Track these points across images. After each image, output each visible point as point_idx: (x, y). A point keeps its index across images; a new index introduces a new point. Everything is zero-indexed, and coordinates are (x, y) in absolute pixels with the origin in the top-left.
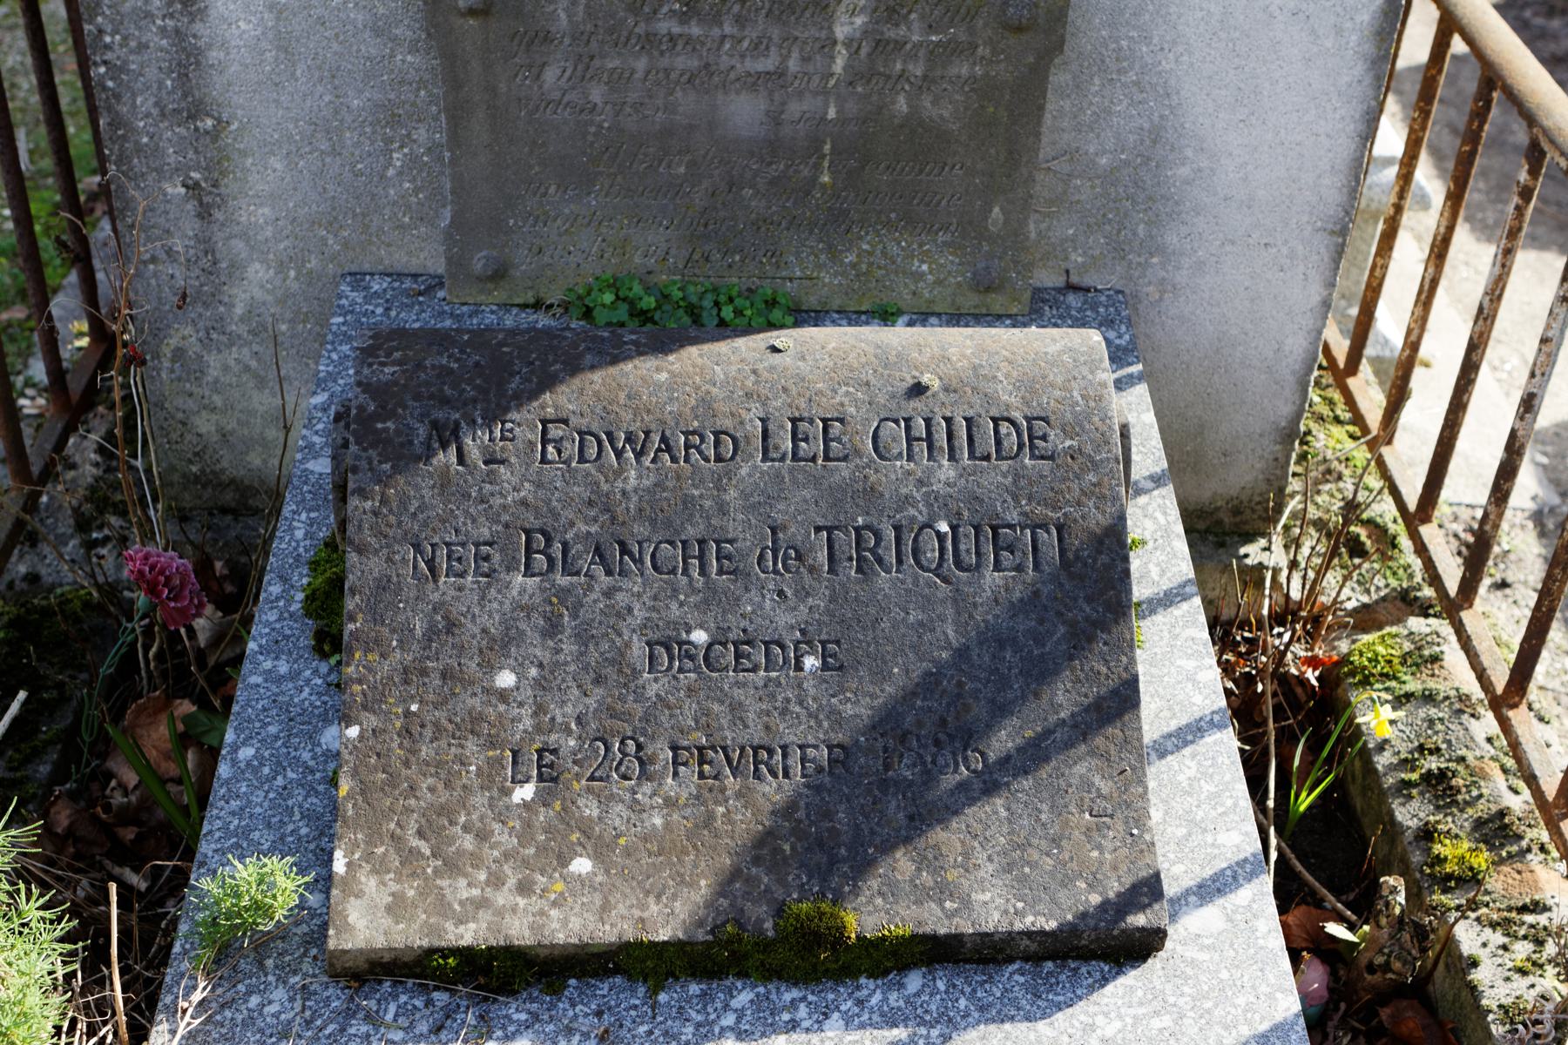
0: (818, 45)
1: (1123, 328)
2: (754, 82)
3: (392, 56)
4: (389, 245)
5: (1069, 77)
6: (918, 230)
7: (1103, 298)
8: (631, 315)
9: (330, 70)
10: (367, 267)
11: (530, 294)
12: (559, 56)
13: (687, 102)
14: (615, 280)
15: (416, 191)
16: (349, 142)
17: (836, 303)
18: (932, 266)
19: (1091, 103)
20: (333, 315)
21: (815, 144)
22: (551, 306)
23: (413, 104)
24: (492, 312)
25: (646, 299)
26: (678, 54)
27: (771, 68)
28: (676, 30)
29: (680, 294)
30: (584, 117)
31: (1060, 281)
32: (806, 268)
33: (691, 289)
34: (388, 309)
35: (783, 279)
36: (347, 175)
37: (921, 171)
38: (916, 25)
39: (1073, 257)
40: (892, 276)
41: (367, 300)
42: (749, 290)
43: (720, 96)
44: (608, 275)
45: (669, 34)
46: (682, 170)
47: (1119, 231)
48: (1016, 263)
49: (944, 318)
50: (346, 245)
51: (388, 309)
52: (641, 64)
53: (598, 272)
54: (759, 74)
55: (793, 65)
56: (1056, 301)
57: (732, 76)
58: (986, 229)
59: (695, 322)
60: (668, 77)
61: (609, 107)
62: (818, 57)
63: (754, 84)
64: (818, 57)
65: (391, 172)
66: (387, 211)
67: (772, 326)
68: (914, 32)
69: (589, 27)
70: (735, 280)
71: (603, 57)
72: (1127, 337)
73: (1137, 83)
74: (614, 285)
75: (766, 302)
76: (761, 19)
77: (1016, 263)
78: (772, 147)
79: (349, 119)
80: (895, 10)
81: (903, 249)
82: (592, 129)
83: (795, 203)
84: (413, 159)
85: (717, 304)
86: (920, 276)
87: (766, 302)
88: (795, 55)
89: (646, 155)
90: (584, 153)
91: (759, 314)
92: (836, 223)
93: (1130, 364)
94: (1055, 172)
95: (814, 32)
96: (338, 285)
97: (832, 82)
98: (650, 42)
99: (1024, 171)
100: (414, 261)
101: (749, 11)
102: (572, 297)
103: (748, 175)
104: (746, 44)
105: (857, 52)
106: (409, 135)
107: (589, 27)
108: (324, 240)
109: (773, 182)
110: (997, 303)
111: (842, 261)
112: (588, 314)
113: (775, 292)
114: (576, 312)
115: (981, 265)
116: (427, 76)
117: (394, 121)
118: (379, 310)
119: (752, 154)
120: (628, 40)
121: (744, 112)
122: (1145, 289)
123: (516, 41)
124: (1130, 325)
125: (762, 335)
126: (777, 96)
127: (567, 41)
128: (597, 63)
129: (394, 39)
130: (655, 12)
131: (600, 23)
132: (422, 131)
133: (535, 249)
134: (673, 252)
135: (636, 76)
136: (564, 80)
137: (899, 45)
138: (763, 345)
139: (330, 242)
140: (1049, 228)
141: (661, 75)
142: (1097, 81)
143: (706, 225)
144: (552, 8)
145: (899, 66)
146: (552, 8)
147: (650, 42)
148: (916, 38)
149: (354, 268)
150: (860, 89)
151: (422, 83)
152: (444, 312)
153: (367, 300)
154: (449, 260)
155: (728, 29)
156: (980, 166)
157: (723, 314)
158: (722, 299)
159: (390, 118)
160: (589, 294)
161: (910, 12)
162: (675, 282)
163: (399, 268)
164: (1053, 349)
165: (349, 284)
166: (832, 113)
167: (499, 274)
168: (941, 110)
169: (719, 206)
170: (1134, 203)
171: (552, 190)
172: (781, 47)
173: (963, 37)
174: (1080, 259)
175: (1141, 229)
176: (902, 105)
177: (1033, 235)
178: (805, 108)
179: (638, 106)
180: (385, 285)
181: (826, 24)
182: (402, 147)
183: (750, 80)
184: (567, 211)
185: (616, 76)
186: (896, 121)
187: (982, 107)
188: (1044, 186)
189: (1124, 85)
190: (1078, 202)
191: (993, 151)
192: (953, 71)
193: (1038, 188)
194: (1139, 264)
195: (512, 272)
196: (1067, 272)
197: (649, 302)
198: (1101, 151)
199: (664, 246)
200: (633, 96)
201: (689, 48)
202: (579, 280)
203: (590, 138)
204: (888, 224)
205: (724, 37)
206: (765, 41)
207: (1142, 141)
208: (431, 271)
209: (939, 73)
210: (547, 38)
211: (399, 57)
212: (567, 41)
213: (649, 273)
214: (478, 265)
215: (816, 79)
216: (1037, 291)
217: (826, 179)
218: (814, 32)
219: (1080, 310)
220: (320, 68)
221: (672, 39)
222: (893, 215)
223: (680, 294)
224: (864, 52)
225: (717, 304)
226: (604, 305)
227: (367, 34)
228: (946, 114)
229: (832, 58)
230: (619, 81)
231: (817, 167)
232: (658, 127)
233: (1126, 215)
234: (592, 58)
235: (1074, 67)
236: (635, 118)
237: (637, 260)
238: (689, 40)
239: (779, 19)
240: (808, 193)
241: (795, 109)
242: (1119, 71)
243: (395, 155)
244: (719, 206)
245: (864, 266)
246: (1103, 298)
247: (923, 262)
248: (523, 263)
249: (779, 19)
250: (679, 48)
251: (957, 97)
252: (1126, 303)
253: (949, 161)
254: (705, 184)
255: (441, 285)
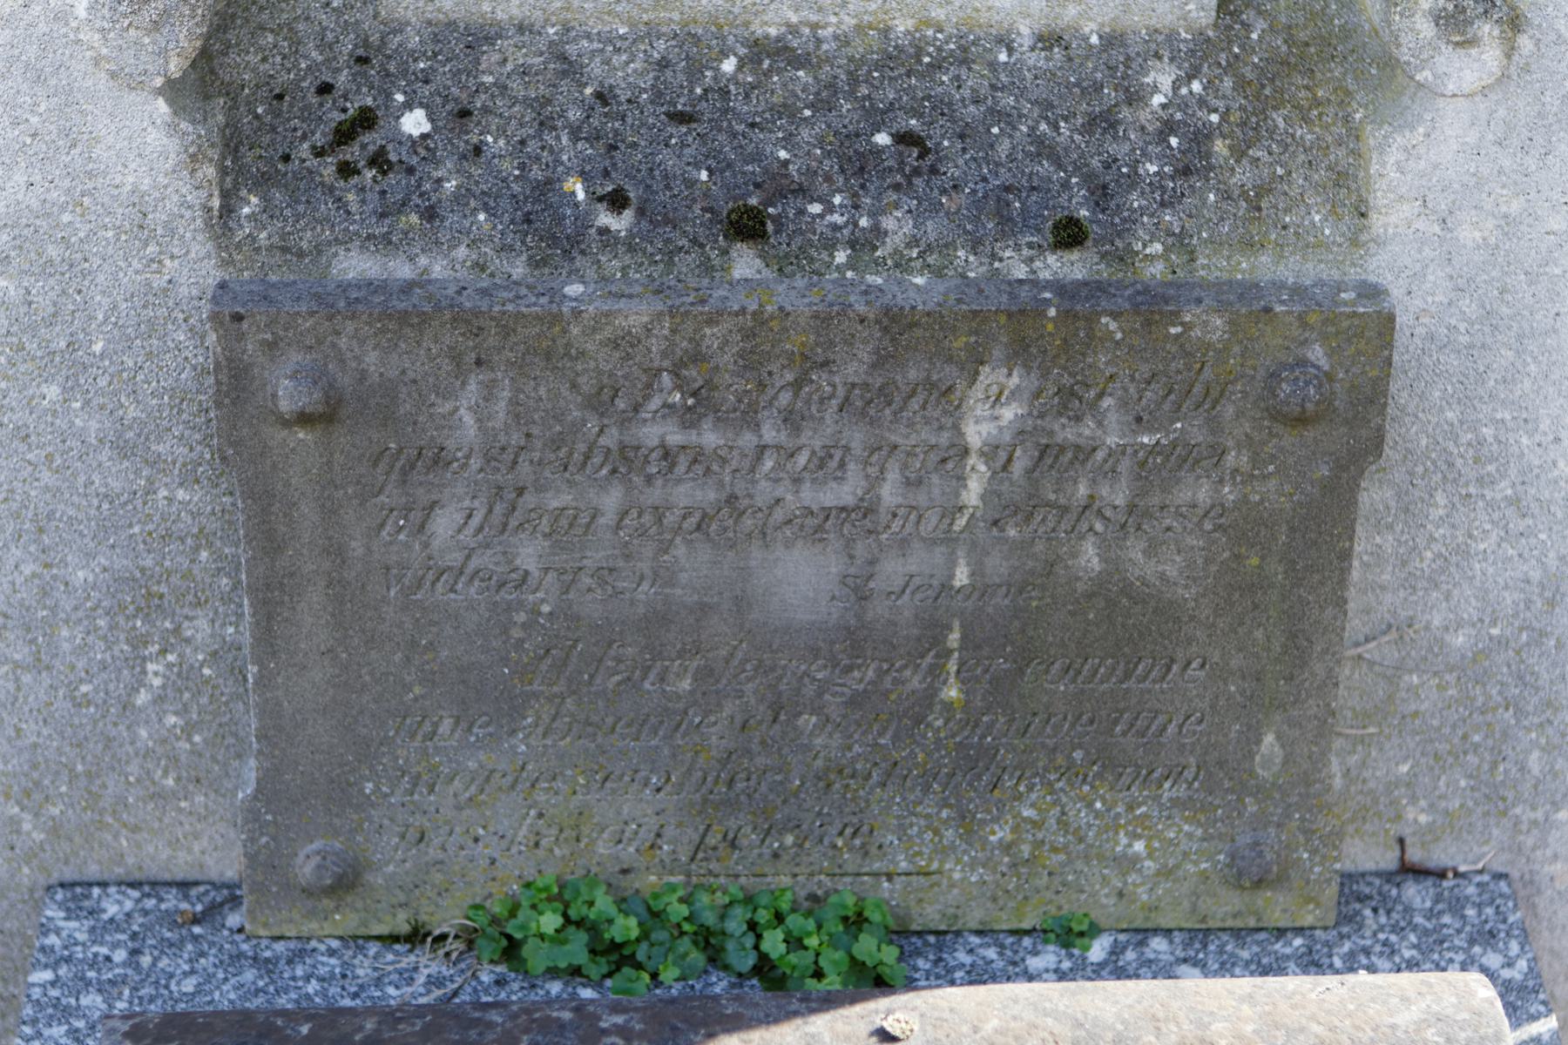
0: (934, 457)
1: (1514, 947)
2: (818, 526)
3: (150, 491)
4: (136, 829)
5: (1389, 493)
6: (1125, 780)
7: (1471, 890)
8: (593, 952)
9: (35, 520)
10: (93, 871)
11: (402, 916)
12: (460, 490)
13: (694, 565)
14: (562, 887)
15: (188, 730)
16: (66, 646)
17: (974, 918)
18: (1149, 848)
19: (1432, 539)
20: (36, 965)
21: (933, 633)
22: (443, 937)
23: (187, 576)
24: (332, 953)
25: (620, 920)
26: (679, 481)
27: (849, 500)
28: (675, 438)
29: (684, 910)
30: (507, 595)
31: (1389, 860)
32: (928, 862)
33: (704, 899)
34: (135, 952)
35: (876, 875)
36: (62, 705)
37: (1127, 675)
38: (1112, 418)
39: (1410, 813)
40: (1079, 865)
41: (96, 935)
42: (813, 898)
43: (756, 553)
44: (549, 879)
45: (663, 445)
46: (686, 685)
47: (1494, 766)
48: (1308, 833)
49: (1178, 937)
50: (55, 830)
51: (135, 952)
52: (611, 500)
53: (530, 873)
54: (827, 513)
55: (889, 493)
56: (1384, 897)
57: (779, 515)
58: (1252, 773)
59: (712, 960)
60: (660, 521)
61: (551, 576)
62: (935, 479)
63: (819, 529)
64: (935, 479)
65: (142, 698)
66: (134, 769)
67: (878, 983)
68: (1110, 430)
69: (516, 439)
70: (786, 880)
71: (540, 489)
72: (1522, 964)
73: (1514, 501)
74: (561, 897)
75: (845, 919)
76: (830, 414)
77: (1308, 833)
78: (853, 640)
79: (67, 604)
80: (1073, 394)
81: (1097, 814)
82: (521, 617)
83: (896, 738)
84: (184, 676)
85: (752, 926)
86: (1129, 863)
87: (845, 919)
88: (893, 475)
89: (619, 660)
90: (505, 660)
91: (834, 943)
92: (972, 772)
93: (1534, 1018)
94: (1371, 663)
95: (926, 435)
96: (38, 907)
97: (961, 522)
98: (627, 459)
99: (1319, 668)
100: (182, 856)
101: (808, 402)
102: (482, 920)
103: (809, 690)
104: (802, 459)
105: (1005, 467)
106: (177, 630)
107: (516, 439)
108: (14, 823)
109: (854, 701)
110: (1276, 907)
111: (985, 841)
112: (511, 950)
113: (861, 899)
114: (487, 949)
115: (1244, 840)
116: (213, 525)
117: (151, 605)
118: (120, 955)
119: (816, 653)
120: (587, 457)
121: (801, 581)
122: (1548, 869)
123: (382, 467)
124: (1525, 938)
125: (858, 1009)
126: (860, 549)
127: (475, 463)
128: (530, 499)
129: (154, 462)
130: (636, 408)
131: (535, 431)
132: (202, 623)
133: (412, 835)
134: (669, 832)
135: (602, 521)
136: (469, 531)
137: (1083, 453)
138: (864, 1029)
139: (26, 827)
140: (1363, 764)
141: (647, 518)
142: (1440, 498)
143: (731, 783)
144: (448, 406)
145: (1083, 490)
146: (448, 406)
147: (627, 459)
148: (1112, 440)
149: (69, 875)
150: (1012, 533)
151: (203, 538)
152: (241, 955)
153: (96, 935)
154: (252, 858)
155: (770, 433)
156: (1236, 662)
157: (765, 946)
158: (763, 916)
159: (144, 602)
160: (513, 914)
161: (1101, 395)
162: (672, 888)
163: (153, 871)
164: (1406, 1018)
165: (60, 905)
166: (962, 577)
167: (345, 882)
168: (1164, 565)
169: (755, 747)
170: (1520, 713)
171: (446, 725)
172: (866, 463)
173: (1198, 436)
174: (1423, 819)
175: (1535, 761)
176: (1090, 557)
177: (1338, 782)
178: (913, 568)
179: (605, 574)
180: (129, 905)
181: (948, 422)
182: (163, 652)
183: (810, 522)
184: (472, 765)
185: (564, 522)
186: (1081, 587)
187: (1237, 557)
188: (1353, 688)
189: (1491, 505)
190: (1416, 714)
191: (1259, 634)
192: (1183, 495)
193: (1341, 691)
194: (1535, 823)
195: (369, 877)
196: (1401, 841)
197: (626, 927)
198: (1454, 620)
199: (652, 823)
200: (595, 557)
201: (699, 469)
202: (494, 888)
203: (516, 633)
204: (1069, 771)
205: (762, 449)
206: (838, 454)
207: (1528, 603)
208: (213, 875)
209: (1155, 500)
210: (440, 460)
211: (163, 493)
212: (475, 463)
213: (625, 872)
214: (305, 869)
215: (932, 518)
216: (1348, 878)
217: (953, 693)
218: (926, 435)
219: (1430, 914)
220: (16, 516)
221: (667, 454)
222: (1078, 755)
223: (684, 910)
224: (1018, 467)
225: (752, 926)
226: (542, 937)
227: (105, 455)
228: (1171, 572)
229: (961, 479)
230: (568, 531)
231: (936, 672)
232: (641, 610)
233: (1505, 734)
234: (520, 491)
235: (1399, 475)
236: (599, 594)
237: (602, 849)
238: (698, 456)
239: (864, 414)
240: (919, 720)
241: (893, 570)
242: (1480, 481)
243: (151, 667)
244: (755, 747)
245: (1026, 850)
246: (1471, 890)
247: (1135, 836)
248: (390, 861)
249: (864, 414)
250: (681, 469)
251: (1191, 541)
252: (1514, 896)
253: (1180, 655)
254: (729, 708)
255: (234, 901)
